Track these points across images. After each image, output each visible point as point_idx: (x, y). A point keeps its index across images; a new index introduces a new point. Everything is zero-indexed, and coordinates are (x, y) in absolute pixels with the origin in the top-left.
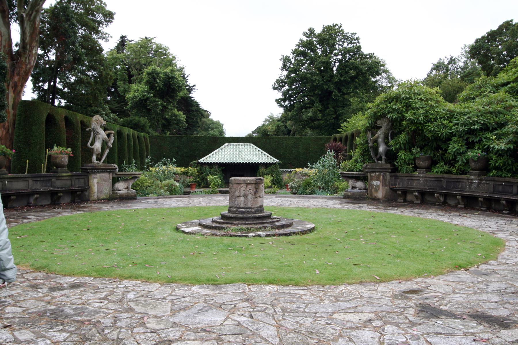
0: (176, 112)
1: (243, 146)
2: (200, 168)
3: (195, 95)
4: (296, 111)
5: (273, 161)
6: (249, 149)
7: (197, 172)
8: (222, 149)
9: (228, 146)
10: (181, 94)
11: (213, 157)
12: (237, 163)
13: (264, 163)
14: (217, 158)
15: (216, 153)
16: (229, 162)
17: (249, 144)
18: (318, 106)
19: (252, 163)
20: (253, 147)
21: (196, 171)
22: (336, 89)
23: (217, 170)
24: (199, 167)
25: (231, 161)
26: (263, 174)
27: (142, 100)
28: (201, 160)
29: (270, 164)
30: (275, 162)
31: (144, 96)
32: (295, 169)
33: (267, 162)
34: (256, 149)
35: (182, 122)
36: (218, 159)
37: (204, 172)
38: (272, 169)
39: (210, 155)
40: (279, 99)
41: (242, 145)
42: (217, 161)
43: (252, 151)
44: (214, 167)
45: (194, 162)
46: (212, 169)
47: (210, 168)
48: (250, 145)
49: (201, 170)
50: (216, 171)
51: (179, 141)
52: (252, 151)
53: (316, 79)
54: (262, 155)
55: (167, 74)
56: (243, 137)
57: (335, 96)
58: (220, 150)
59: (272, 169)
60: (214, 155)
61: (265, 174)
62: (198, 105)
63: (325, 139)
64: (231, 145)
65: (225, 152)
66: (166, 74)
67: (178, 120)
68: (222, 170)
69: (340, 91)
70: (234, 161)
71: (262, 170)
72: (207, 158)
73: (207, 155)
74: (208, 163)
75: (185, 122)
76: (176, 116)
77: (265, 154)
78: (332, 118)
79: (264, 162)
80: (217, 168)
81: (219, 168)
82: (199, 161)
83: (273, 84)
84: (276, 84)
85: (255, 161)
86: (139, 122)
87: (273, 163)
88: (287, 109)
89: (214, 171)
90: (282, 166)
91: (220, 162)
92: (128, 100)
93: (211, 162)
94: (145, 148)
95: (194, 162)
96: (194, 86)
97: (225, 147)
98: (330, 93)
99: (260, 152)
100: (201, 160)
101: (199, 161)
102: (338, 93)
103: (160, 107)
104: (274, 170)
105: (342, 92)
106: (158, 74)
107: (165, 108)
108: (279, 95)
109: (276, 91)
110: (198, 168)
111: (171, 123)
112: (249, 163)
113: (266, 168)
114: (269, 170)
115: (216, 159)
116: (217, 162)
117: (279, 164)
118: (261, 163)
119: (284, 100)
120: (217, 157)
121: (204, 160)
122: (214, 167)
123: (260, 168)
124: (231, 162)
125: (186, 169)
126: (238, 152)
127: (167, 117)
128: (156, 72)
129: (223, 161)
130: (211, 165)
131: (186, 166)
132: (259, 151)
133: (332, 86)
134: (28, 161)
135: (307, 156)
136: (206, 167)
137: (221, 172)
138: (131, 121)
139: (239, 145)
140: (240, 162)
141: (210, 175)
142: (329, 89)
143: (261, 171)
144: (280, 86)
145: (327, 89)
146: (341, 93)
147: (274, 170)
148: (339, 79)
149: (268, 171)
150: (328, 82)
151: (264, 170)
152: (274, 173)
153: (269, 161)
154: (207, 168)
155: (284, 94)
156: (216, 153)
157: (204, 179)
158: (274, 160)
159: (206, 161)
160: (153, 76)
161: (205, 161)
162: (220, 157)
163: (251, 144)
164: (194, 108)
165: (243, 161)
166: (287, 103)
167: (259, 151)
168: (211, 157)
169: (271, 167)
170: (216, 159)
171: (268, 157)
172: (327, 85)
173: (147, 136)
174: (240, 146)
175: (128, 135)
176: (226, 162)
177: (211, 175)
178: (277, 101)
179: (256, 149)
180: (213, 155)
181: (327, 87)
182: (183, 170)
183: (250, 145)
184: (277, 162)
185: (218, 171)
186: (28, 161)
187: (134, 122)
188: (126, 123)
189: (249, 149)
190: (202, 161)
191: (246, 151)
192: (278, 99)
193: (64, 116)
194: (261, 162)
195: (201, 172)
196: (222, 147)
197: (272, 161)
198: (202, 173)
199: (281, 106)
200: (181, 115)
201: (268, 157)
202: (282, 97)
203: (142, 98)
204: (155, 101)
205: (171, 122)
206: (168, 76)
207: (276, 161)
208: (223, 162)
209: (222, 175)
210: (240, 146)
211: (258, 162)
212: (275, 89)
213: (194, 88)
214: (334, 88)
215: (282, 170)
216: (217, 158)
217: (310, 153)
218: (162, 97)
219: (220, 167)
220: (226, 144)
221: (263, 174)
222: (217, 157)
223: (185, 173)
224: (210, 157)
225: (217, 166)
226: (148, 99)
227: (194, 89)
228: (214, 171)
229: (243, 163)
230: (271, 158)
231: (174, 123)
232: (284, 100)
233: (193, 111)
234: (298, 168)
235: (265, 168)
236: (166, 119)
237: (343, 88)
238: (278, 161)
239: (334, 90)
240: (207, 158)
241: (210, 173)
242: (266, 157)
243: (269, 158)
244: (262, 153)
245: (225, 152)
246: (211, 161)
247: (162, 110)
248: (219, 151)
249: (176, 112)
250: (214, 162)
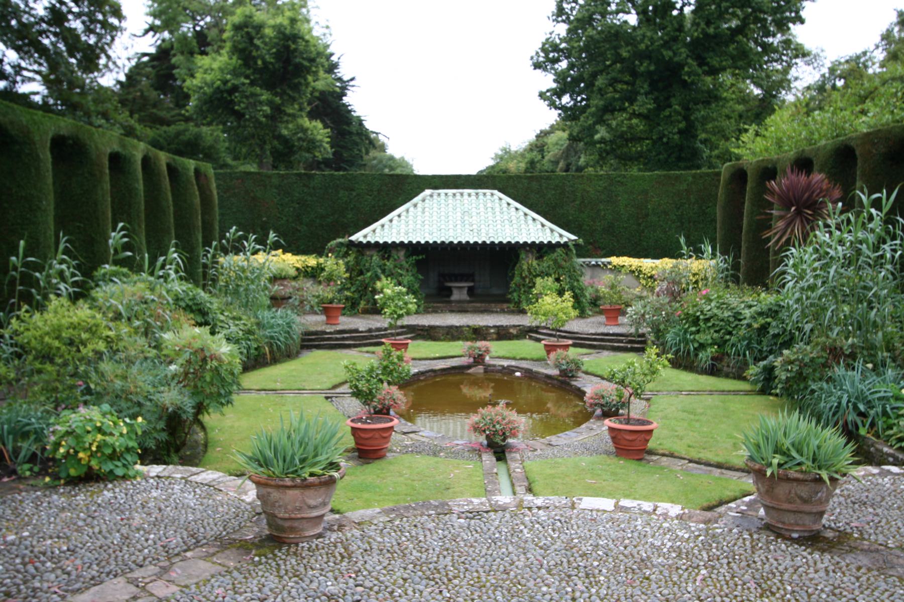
0: (306, 122)
1: (473, 197)
2: (356, 258)
3: (354, 101)
4: (593, 115)
5: (558, 239)
6: (489, 205)
7: (346, 272)
8: (415, 206)
9: (431, 196)
10: (321, 83)
11: (391, 227)
12: (460, 242)
13: (534, 243)
14: (403, 231)
15: (399, 216)
16: (435, 242)
17: (488, 192)
18: (644, 105)
19: (501, 243)
20: (500, 199)
21: (343, 268)
22: (692, 59)
23: (404, 263)
24: (353, 256)
25: (443, 239)
26: (530, 273)
27: (222, 92)
28: (358, 237)
29: (551, 247)
30: (565, 239)
31: (225, 82)
32: (608, 260)
33: (541, 239)
34: (509, 204)
35: (318, 144)
36: (407, 233)
37: (368, 271)
38: (555, 261)
39: (384, 220)
40: (548, 91)
41: (469, 195)
42: (402, 240)
43: (498, 209)
44: (394, 253)
45: (340, 240)
46: (388, 259)
47: (383, 258)
48: (492, 195)
49: (357, 263)
50: (401, 268)
51: (305, 185)
52: (498, 209)
53: (644, 36)
54: (526, 221)
55: (282, 29)
56: (469, 176)
57: (689, 74)
58: (412, 209)
59: (555, 261)
60: (394, 222)
61: (537, 276)
62: (360, 122)
63: (690, 179)
64: (439, 195)
65: (423, 212)
66: (279, 29)
67: (309, 142)
68: (418, 264)
69: (702, 62)
70: (451, 239)
71: (528, 262)
72: (374, 231)
73: (377, 220)
74: (377, 243)
75: (327, 143)
76: (304, 130)
77: (534, 220)
78: (676, 130)
79: (533, 239)
80: (402, 258)
81: (407, 256)
82: (353, 238)
83: (534, 54)
84: (542, 54)
85: (509, 239)
86: (198, 137)
87: (558, 244)
88: (570, 115)
89: (395, 266)
90: (581, 251)
91: (410, 242)
92: (191, 92)
93: (385, 243)
94: (197, 201)
95: (340, 240)
96: (352, 79)
97: (424, 200)
98: (681, 66)
99: (521, 213)
100: (358, 237)
101: (353, 238)
102: (697, 68)
103: (266, 109)
104: (564, 263)
105: (707, 64)
106: (259, 27)
107: (277, 112)
108: (548, 81)
109: (538, 71)
110: (350, 258)
111: (295, 149)
112: (493, 243)
113: (540, 258)
114: (547, 262)
115: (399, 233)
116: (402, 243)
117: (577, 245)
118: (525, 243)
119: (559, 93)
120: (403, 226)
121: (365, 236)
122: (394, 253)
123: (523, 256)
124: (443, 242)
125: (321, 260)
126: (459, 214)
127: (285, 132)
128: (255, 24)
129: (418, 239)
130: (386, 249)
131: (320, 253)
132: (517, 209)
133: (683, 50)
134: (22, 243)
135: (639, 225)
136: (371, 256)
137: (415, 270)
138: (178, 134)
139: (462, 194)
140: (468, 242)
141: (384, 278)
142: (676, 59)
143: (525, 267)
144: (548, 59)
145: (671, 58)
146: (706, 68)
147: (564, 263)
148: (702, 33)
149: (545, 265)
150: (672, 43)
151: (535, 263)
152: (561, 271)
153: (549, 239)
154: (376, 258)
155: (560, 77)
156: (399, 216)
157: (366, 288)
158: (561, 236)
159: (372, 239)
160: (248, 33)
161: (369, 239)
162: (411, 227)
163: (496, 192)
164: (354, 129)
165: (476, 239)
166: (566, 99)
167: (517, 209)
168: (386, 227)
169: (554, 256)
170: (399, 233)
171: (543, 225)
172: (670, 48)
173: (209, 169)
174: (466, 196)
175: (117, 161)
176: (427, 242)
177: (387, 277)
178: (542, 95)
179: (509, 204)
180: (391, 221)
181: (670, 53)
182: (312, 261)
183: (492, 195)
184: (570, 240)
185: (407, 266)
186: (22, 243)
187: (185, 138)
188: (164, 138)
189: (489, 205)
190: (361, 239)
191: (482, 209)
192: (544, 90)
193: (50, 135)
194: (525, 240)
195: (355, 271)
196: (415, 200)
197: (555, 239)
198: (361, 273)
199: (552, 105)
200: (319, 130)
201: (543, 225)
202: (554, 85)
203: (222, 87)
204: (253, 95)
205: (293, 146)
206: (284, 34)
207: (568, 236)
208: (418, 243)
209: (416, 278)
210: (466, 196)
211: (517, 240)
212: (537, 66)
213: (351, 83)
214: (688, 56)
215: (581, 260)
216: (403, 231)
217: (647, 215)
218: (269, 86)
219: (412, 254)
220: (428, 192)
221: (530, 273)
222: (403, 226)
223: (313, 274)
224: (383, 226)
225: (402, 254)
226: (235, 89)
227: (353, 86)
228: (395, 266)
229: (476, 243)
230: (552, 231)
231: (300, 148)
232: (559, 93)
233: (350, 133)
234: (618, 256)
235: (537, 259)
236: (280, 137)
237: (711, 54)
238: (573, 237)
239: (690, 61)
240: (374, 231)
241: (384, 271)
242: (540, 226)
243: (548, 231)
244: (526, 215)
245: (423, 212)
246: (386, 239)
247: (271, 118)
248: (407, 211)
249: (306, 122)
250: (394, 243)
